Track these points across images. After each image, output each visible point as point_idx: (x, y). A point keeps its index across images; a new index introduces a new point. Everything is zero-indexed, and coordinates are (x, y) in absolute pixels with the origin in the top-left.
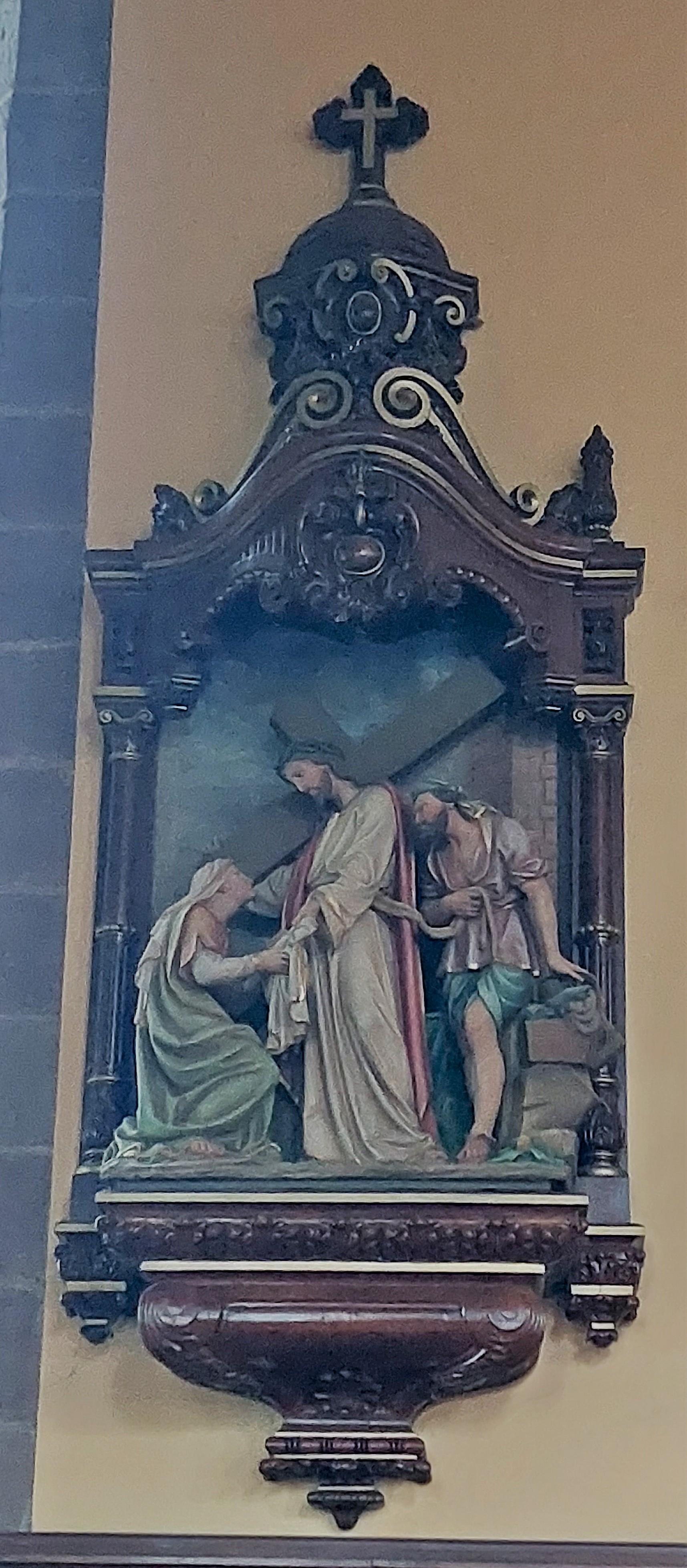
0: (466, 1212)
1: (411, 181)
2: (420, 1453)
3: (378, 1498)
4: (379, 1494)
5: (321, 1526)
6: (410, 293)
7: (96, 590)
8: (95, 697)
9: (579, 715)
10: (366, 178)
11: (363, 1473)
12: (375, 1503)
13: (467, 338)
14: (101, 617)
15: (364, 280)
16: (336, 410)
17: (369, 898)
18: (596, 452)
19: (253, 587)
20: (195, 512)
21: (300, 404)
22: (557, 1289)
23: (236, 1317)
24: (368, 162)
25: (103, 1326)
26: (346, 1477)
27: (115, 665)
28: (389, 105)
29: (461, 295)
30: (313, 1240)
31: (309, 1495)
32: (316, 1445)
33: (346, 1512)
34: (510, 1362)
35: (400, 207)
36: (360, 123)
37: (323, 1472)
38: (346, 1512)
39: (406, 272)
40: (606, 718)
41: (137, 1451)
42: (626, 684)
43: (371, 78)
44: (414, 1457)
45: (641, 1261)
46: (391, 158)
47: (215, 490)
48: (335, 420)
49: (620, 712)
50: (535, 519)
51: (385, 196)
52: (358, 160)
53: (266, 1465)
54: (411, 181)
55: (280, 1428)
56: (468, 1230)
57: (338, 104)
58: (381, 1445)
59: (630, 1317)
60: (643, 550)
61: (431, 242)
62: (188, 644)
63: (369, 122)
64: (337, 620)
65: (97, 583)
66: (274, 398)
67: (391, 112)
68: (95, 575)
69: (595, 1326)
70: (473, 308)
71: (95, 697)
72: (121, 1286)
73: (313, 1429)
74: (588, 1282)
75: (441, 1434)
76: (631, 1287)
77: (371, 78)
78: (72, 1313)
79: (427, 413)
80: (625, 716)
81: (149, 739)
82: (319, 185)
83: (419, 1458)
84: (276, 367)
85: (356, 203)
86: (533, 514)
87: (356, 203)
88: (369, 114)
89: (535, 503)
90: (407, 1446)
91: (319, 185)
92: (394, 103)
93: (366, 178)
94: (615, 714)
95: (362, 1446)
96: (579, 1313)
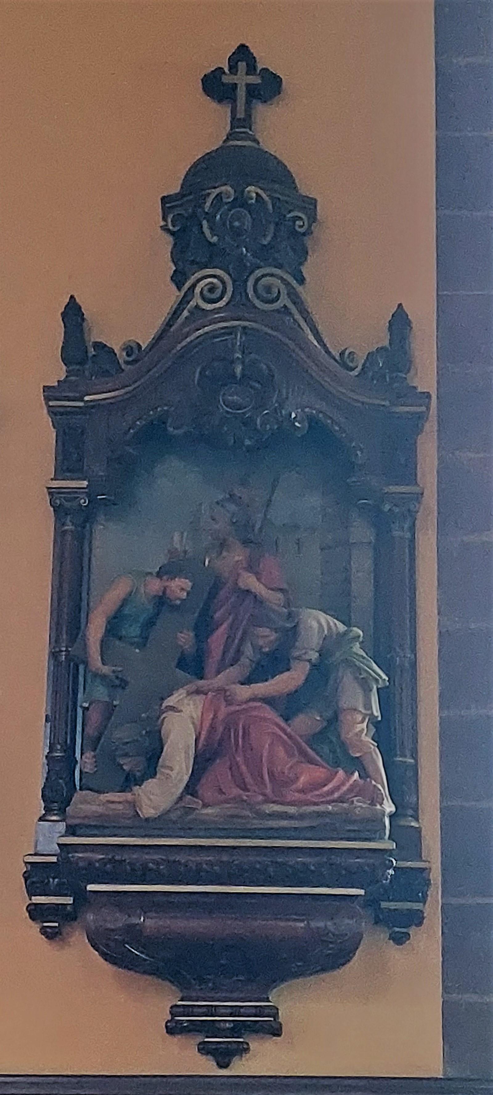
0: (146, 850)
1: (276, 130)
2: (276, 1016)
3: (245, 1046)
4: (248, 1044)
5: (207, 1066)
8: (48, 488)
10: (241, 124)
11: (238, 1029)
12: (243, 1050)
13: (308, 242)
15: (240, 201)
16: (255, 291)
18: (400, 322)
21: (198, 290)
25: (56, 927)
28: (254, 74)
29: (303, 209)
30: (97, 869)
32: (204, 1010)
33: (223, 1056)
34: (328, 956)
35: (263, 146)
37: (211, 1029)
38: (223, 1056)
43: (243, 52)
44: (272, 1019)
46: (260, 109)
48: (221, 304)
50: (355, 373)
52: (234, 112)
54: (276, 130)
56: (149, 863)
58: (201, 1010)
59: (420, 924)
60: (44, 386)
63: (242, 84)
65: (51, 409)
66: (178, 279)
67: (255, 80)
68: (51, 403)
70: (313, 218)
72: (70, 900)
75: (295, 1002)
76: (421, 904)
77: (243, 52)
78: (32, 918)
79: (285, 300)
81: (87, 518)
82: (208, 127)
83: (275, 1020)
85: (231, 143)
86: (352, 369)
87: (231, 143)
88: (242, 79)
90: (267, 1011)
91: (208, 127)
93: (241, 124)
94: (408, 510)
95: (235, 1011)
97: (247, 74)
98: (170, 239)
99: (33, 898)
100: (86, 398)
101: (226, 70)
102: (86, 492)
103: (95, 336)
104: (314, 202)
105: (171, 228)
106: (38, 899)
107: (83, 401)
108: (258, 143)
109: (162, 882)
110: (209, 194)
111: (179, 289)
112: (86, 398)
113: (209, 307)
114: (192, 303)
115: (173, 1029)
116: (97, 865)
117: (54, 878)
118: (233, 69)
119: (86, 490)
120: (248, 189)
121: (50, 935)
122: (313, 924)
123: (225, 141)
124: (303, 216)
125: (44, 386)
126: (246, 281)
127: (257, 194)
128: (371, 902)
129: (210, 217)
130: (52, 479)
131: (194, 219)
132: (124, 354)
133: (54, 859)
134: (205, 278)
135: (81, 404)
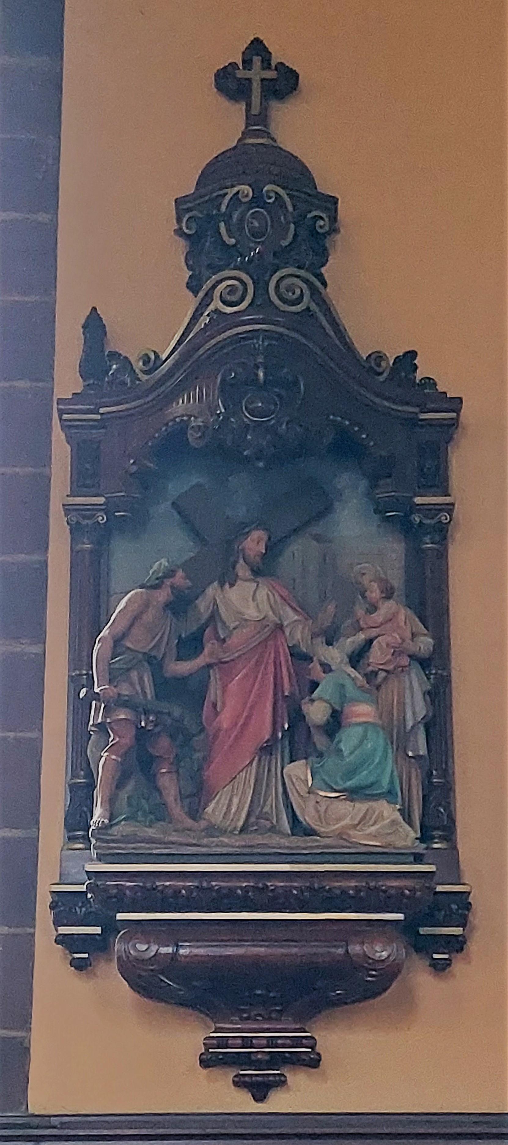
1: (294, 128)
2: (313, 1047)
3: (283, 1079)
4: (285, 1077)
5: (243, 1103)
6: (290, 208)
7: (66, 426)
9: (416, 518)
10: (258, 122)
11: (277, 1060)
12: (281, 1082)
14: (69, 448)
17: (259, 611)
19: (183, 428)
20: (137, 371)
21: (217, 293)
22: (408, 930)
23: (182, 951)
24: (255, 111)
26: (257, 1065)
27: (82, 480)
29: (326, 209)
31: (235, 1076)
33: (260, 1090)
36: (249, 80)
38: (260, 1090)
39: (288, 194)
40: (435, 520)
41: (99, 1046)
42: (450, 496)
43: (257, 47)
44: (310, 1050)
45: (469, 910)
46: (274, 104)
47: (152, 356)
49: (446, 516)
51: (269, 135)
52: (249, 106)
53: (204, 1057)
54: (294, 128)
55: (213, 1030)
57: (234, 65)
60: (460, 399)
61: (305, 172)
62: (134, 468)
63: (259, 80)
64: (245, 453)
66: (193, 286)
68: (65, 416)
69: (435, 956)
70: (334, 219)
71: (63, 505)
72: (98, 930)
73: (233, 1031)
74: (434, 923)
75: (333, 1038)
77: (257, 47)
80: (448, 517)
81: (103, 536)
82: (224, 126)
84: (192, 259)
88: (257, 74)
89: (383, 364)
91: (224, 126)
92: (273, 68)
93: (258, 122)
95: (272, 1042)
96: (422, 946)
97: (263, 69)
98: (182, 245)
99: (59, 928)
100: (102, 410)
101: (241, 68)
102: (103, 510)
103: (112, 346)
104: (334, 201)
105: (186, 231)
106: (64, 930)
107: (98, 413)
108: (275, 141)
109: (303, 910)
110: (226, 194)
111: (196, 293)
112: (102, 410)
113: (229, 310)
114: (212, 307)
115: (205, 1062)
116: (128, 892)
117: (81, 908)
118: (247, 63)
119: (103, 507)
120: (265, 189)
121: (79, 966)
122: (170, 950)
123: (240, 140)
124: (324, 215)
125: (59, 399)
126: (267, 284)
127: (276, 193)
128: (408, 930)
129: (227, 217)
130: (67, 496)
131: (212, 220)
132: (141, 363)
133: (84, 888)
134: (226, 280)
135: (98, 417)
